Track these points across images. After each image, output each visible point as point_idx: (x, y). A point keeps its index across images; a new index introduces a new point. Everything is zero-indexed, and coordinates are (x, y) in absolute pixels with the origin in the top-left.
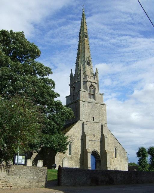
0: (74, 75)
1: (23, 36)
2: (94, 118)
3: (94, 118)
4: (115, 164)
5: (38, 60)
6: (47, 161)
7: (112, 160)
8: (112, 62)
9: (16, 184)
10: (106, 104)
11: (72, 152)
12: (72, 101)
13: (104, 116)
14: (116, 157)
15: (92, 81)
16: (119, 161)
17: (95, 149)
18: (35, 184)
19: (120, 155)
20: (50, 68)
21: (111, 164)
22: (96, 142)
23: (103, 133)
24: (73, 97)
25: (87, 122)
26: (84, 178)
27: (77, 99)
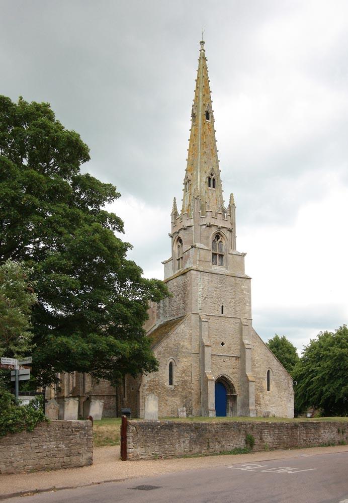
0: (180, 213)
1: (49, 115)
2: (222, 307)
3: (222, 307)
4: (267, 402)
5: (85, 169)
6: (125, 397)
7: (261, 396)
8: (287, 428)
9: (11, 462)
10: (250, 276)
11: (174, 380)
12: (177, 272)
13: (245, 304)
14: (268, 390)
15: (220, 225)
16: (274, 396)
17: (224, 372)
18: (61, 460)
19: (278, 385)
20: (114, 185)
21: (258, 402)
22: (227, 359)
23: (243, 341)
24: (177, 262)
25: (208, 317)
26: (184, 442)
27: (65, 140)
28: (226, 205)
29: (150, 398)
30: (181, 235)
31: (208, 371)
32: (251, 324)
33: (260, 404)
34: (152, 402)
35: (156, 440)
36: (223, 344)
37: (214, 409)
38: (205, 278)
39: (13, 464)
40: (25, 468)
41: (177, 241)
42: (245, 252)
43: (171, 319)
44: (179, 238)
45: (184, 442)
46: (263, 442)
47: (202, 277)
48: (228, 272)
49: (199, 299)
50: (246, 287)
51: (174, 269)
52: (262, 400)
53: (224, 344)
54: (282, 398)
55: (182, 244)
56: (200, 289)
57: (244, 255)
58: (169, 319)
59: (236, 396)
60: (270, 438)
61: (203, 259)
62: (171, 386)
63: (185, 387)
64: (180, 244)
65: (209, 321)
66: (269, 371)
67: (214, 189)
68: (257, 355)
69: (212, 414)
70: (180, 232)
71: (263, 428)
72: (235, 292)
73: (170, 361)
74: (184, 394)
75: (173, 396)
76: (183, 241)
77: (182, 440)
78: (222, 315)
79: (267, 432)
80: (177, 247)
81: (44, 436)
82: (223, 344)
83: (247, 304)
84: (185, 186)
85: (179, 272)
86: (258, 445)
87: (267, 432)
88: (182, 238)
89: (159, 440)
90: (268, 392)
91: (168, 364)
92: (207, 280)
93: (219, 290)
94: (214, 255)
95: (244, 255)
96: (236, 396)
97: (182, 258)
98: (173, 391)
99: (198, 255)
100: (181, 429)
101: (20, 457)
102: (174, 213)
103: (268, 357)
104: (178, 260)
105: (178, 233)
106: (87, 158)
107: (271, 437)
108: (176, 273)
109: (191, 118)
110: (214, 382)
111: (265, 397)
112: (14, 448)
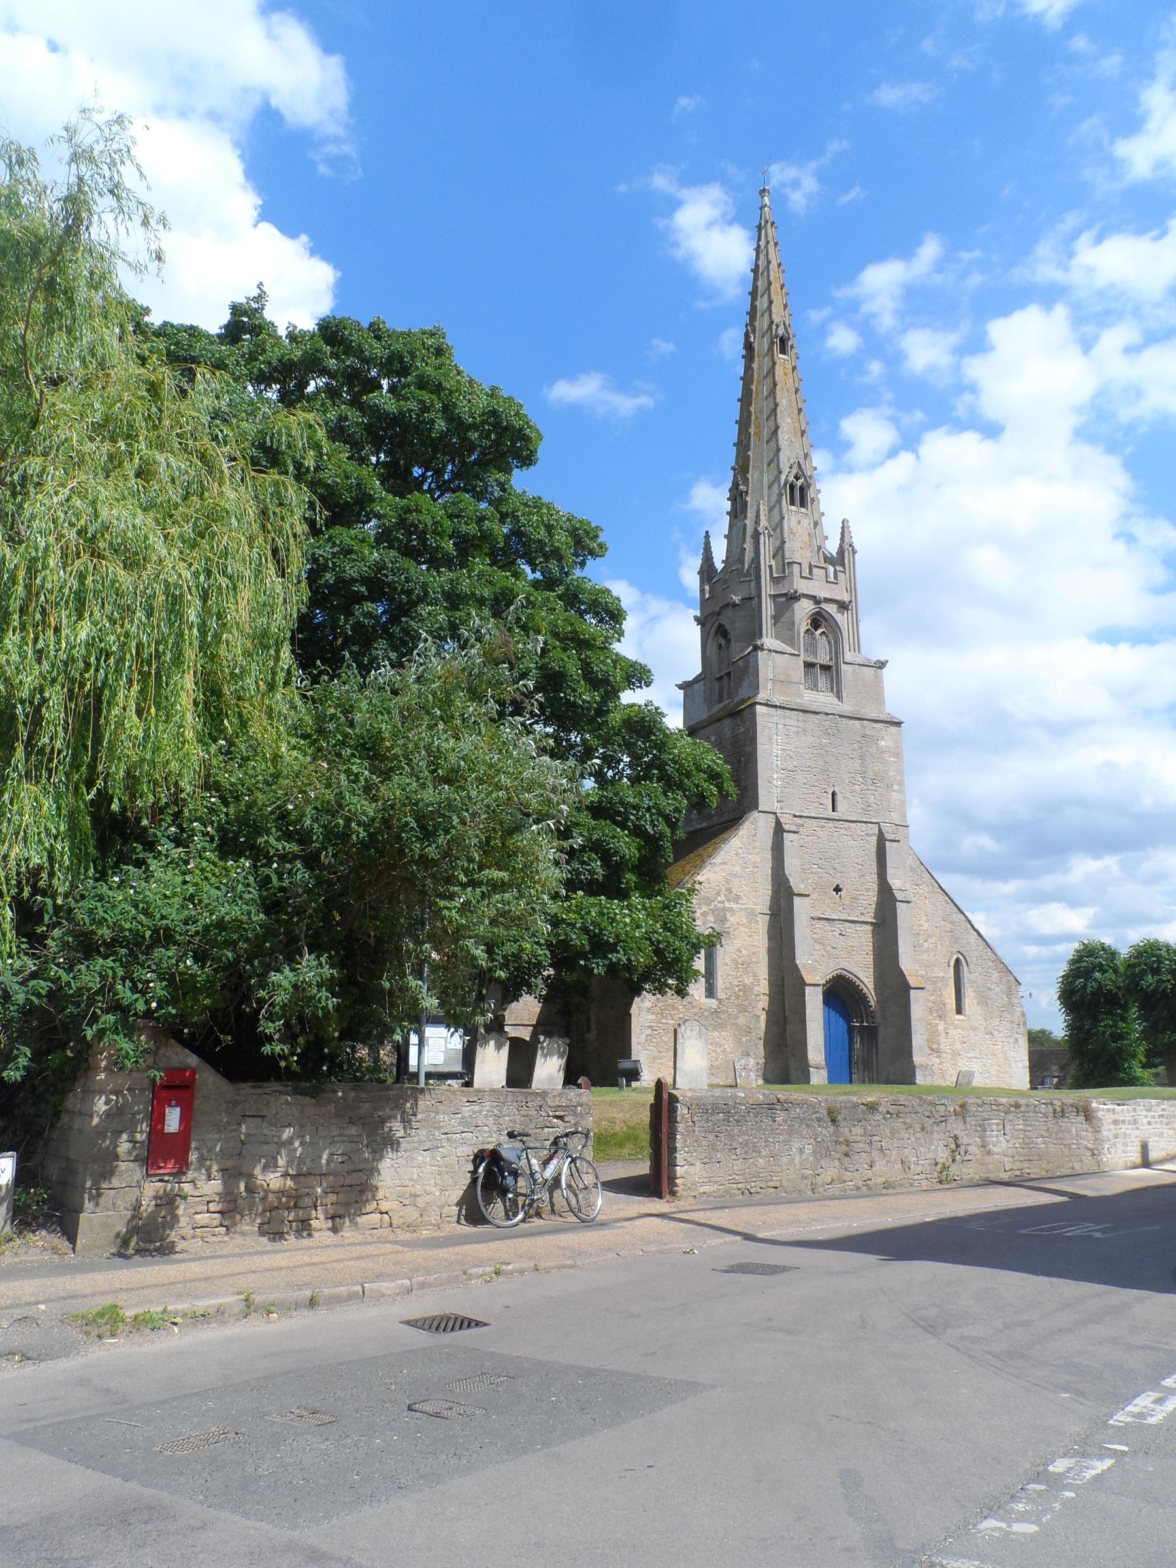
0: (719, 566)
2: (834, 794)
3: (834, 794)
4: (958, 1046)
6: (589, 1030)
7: (941, 1027)
11: (720, 984)
14: (959, 1011)
15: (822, 594)
16: (975, 1029)
17: (845, 965)
19: (983, 1000)
21: (934, 1046)
22: (850, 929)
24: (717, 685)
28: (832, 547)
29: (688, 1032)
30: (724, 620)
31: (803, 959)
32: (907, 837)
33: (937, 1051)
34: (693, 1041)
35: (735, 1145)
36: (837, 889)
37: (823, 1062)
38: (788, 722)
39: (419, 1199)
40: (444, 1211)
41: (716, 634)
42: (882, 659)
43: (705, 824)
44: (721, 626)
45: (801, 1151)
46: (989, 1153)
47: (782, 721)
48: (846, 707)
49: (775, 776)
50: (891, 744)
51: (709, 702)
52: (942, 1040)
53: (840, 890)
54: (995, 1033)
55: (729, 641)
56: (777, 750)
57: (881, 665)
58: (698, 826)
59: (876, 1028)
60: (1004, 1144)
61: (782, 678)
62: (709, 1001)
63: (746, 1003)
64: (722, 641)
65: (802, 830)
66: (958, 960)
67: (803, 510)
68: (924, 918)
69: (818, 1077)
70: (725, 612)
71: (985, 1115)
72: (862, 758)
73: (955, 957)
74: (742, 1020)
75: (715, 1029)
76: (732, 634)
77: (796, 1145)
78: (834, 815)
79: (997, 1125)
80: (715, 649)
81: (486, 1129)
82: (837, 889)
83: (896, 787)
84: (733, 505)
85: (722, 709)
86: (977, 1160)
87: (997, 1125)
88: (728, 627)
89: (745, 1144)
90: (958, 1017)
91: (952, 963)
92: (794, 729)
93: (823, 752)
94: (809, 666)
95: (881, 665)
96: (876, 1028)
97: (728, 674)
98: (716, 1013)
99: (770, 669)
100: (793, 1114)
101: (432, 1182)
102: (705, 568)
103: (953, 923)
104: (720, 679)
105: (719, 614)
106: (527, 460)
107: (1007, 1141)
108: (715, 710)
109: (744, 352)
110: (820, 989)
111: (952, 1032)
112: (420, 1158)
